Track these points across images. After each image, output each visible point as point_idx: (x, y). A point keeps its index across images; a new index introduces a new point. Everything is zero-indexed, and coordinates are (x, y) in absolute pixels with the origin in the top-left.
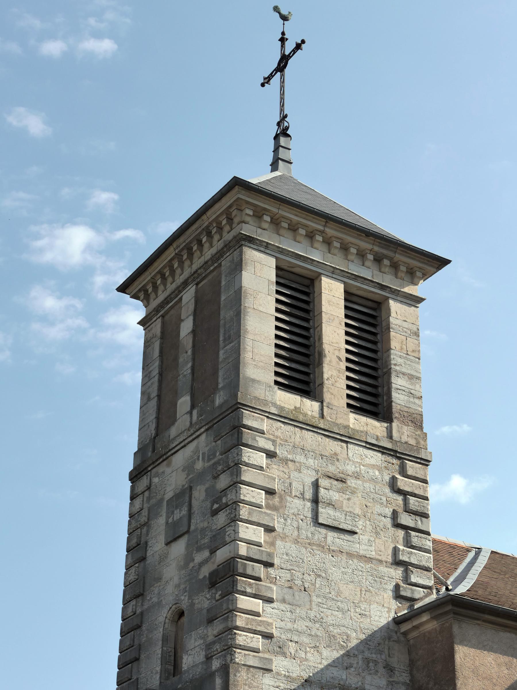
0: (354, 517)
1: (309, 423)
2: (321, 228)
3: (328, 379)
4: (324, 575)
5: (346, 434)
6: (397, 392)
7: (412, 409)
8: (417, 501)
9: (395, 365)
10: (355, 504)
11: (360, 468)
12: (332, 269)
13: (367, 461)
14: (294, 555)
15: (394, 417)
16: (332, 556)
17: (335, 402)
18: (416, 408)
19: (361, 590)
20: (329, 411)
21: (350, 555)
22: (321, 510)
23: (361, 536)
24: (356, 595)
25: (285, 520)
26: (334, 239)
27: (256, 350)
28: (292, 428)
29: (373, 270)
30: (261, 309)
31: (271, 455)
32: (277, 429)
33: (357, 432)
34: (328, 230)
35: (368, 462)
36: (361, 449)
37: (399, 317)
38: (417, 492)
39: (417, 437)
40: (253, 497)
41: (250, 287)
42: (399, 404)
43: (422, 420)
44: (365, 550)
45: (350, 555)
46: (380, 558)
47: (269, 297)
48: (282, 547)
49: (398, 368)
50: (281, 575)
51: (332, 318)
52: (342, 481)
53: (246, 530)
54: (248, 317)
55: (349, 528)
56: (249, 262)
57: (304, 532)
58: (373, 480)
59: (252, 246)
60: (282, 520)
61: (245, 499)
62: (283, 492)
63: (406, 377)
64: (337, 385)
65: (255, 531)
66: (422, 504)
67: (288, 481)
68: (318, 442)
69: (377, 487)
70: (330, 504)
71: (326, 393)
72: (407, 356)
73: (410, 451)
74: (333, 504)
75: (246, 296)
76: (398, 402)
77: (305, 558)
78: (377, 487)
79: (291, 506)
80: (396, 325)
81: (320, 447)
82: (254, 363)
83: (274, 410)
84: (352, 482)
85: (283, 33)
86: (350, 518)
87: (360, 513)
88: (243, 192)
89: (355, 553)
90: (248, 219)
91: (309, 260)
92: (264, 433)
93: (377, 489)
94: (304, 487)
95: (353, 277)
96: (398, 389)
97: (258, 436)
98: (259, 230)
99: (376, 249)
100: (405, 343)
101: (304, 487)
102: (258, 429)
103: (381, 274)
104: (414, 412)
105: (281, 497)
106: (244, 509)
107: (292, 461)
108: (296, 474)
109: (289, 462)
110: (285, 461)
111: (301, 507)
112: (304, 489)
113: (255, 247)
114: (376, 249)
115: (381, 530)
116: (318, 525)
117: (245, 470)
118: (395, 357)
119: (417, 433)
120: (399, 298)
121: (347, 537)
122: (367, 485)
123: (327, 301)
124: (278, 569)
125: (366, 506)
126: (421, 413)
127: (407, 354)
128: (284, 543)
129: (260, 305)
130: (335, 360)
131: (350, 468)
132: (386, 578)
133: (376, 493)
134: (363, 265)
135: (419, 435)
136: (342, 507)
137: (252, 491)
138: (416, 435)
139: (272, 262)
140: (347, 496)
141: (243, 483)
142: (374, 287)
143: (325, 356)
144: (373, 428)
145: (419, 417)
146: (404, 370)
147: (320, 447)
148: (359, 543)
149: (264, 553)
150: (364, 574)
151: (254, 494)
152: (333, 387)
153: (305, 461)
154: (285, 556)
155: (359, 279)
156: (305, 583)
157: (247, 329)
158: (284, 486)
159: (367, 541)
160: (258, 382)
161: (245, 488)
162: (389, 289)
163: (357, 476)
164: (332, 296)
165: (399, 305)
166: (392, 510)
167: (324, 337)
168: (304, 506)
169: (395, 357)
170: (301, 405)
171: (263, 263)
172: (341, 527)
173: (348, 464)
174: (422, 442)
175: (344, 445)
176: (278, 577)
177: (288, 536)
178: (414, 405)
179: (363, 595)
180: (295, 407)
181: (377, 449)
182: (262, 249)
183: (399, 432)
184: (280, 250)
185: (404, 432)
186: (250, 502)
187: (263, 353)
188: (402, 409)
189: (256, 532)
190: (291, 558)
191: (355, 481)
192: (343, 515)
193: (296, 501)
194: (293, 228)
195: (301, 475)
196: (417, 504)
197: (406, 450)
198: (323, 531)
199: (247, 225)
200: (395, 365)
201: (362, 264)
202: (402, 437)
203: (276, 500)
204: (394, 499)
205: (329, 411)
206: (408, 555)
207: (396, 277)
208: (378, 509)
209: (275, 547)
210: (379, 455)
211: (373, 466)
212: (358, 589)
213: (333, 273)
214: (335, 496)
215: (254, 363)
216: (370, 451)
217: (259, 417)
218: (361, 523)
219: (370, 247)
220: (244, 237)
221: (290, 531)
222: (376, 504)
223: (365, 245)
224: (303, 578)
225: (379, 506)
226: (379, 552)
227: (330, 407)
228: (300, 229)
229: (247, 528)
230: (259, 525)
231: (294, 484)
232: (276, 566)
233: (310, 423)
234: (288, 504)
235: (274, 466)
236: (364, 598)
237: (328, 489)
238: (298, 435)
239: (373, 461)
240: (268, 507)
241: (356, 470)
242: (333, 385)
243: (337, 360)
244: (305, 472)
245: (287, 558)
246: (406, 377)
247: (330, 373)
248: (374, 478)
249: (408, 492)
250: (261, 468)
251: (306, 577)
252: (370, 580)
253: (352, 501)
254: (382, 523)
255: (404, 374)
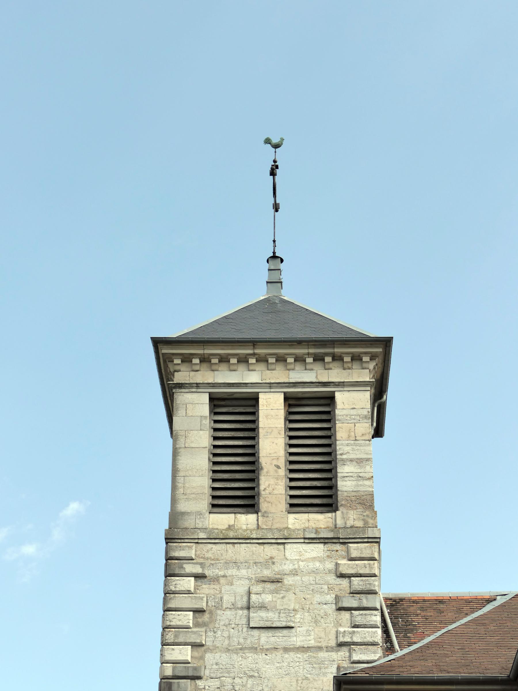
0: (289, 613)
1: (240, 537)
2: (250, 352)
3: (265, 489)
4: (256, 674)
5: (281, 537)
6: (343, 481)
7: (361, 491)
8: (362, 580)
9: (341, 454)
10: (289, 600)
11: (299, 565)
12: (268, 385)
13: (308, 555)
14: (224, 663)
15: (339, 505)
16: (266, 655)
17: (272, 509)
18: (364, 490)
19: (297, 680)
20: (264, 520)
21: (286, 650)
22: (252, 615)
23: (298, 629)
24: (291, 685)
25: (215, 632)
26: (268, 357)
27: (187, 485)
28: (223, 546)
29: (317, 371)
30: (193, 445)
31: (199, 577)
32: (208, 551)
33: (294, 531)
34: (257, 351)
35: (308, 556)
36: (298, 545)
37: (347, 406)
38: (361, 572)
39: (365, 518)
40: (180, 620)
41: (181, 429)
42: (346, 491)
43: (373, 500)
44: (303, 641)
45: (286, 650)
46: (319, 645)
47: (201, 432)
48: (212, 658)
49: (344, 457)
50: (210, 684)
51: (270, 431)
52: (278, 582)
53: (172, 652)
54: (179, 457)
55: (284, 624)
56: (181, 406)
57: (235, 639)
58: (315, 572)
59: (183, 390)
60: (212, 633)
61: (172, 624)
62: (213, 607)
63: (354, 463)
64: (275, 492)
65: (181, 651)
66: (367, 582)
67: (219, 596)
68: (252, 551)
69: (318, 578)
70: (262, 607)
71: (262, 504)
72: (356, 442)
73: (354, 534)
74: (266, 606)
75: (177, 438)
76: (345, 489)
77: (236, 663)
78: (317, 577)
79: (222, 618)
80: (343, 416)
81: (254, 556)
82: (185, 497)
83: (202, 535)
84: (288, 581)
85: (275, 161)
86: (284, 615)
87: (297, 608)
88: (165, 347)
89: (291, 647)
90: (177, 368)
91: (242, 385)
92: (192, 559)
93: (317, 580)
94: (235, 598)
95: (292, 385)
96: (344, 477)
97: (187, 563)
98: (192, 373)
99: (312, 351)
100: (353, 430)
101: (235, 598)
102: (185, 557)
103: (327, 371)
104: (363, 494)
105: (211, 613)
106: (170, 634)
107: (223, 576)
108: (228, 587)
109: (221, 579)
110: (216, 579)
111: (232, 617)
112: (235, 599)
113: (187, 390)
114: (312, 351)
115: (322, 618)
116: (251, 629)
117: (171, 599)
118: (341, 447)
119: (365, 514)
120: (346, 389)
121: (285, 632)
122: (306, 579)
123: (264, 417)
124: (207, 680)
125: (304, 599)
126: (371, 493)
127: (356, 440)
128: (214, 654)
129: (192, 442)
130: (272, 469)
131: (288, 567)
132: (326, 663)
133: (316, 584)
134: (306, 369)
135: (368, 516)
136: (275, 607)
137: (179, 615)
138: (364, 516)
139: (206, 398)
140: (282, 595)
141: (170, 609)
142: (317, 387)
143: (262, 469)
144: (316, 522)
145: (368, 497)
146: (352, 456)
147: (254, 556)
148: (296, 636)
149: (189, 669)
150: (302, 664)
151: (181, 617)
152: (270, 496)
153: (237, 573)
154: (215, 667)
155: (297, 385)
156: (236, 686)
157: (178, 468)
158: (215, 602)
159: (305, 632)
160: (188, 513)
161: (171, 614)
162: (333, 384)
163: (294, 573)
164: (272, 411)
165: (347, 394)
166: (334, 596)
167: (260, 451)
168: (236, 614)
169: (341, 447)
170: (235, 522)
171: (195, 402)
172: (274, 626)
173: (285, 564)
174: (371, 521)
175: (281, 547)
176: (207, 687)
177: (218, 647)
178: (365, 486)
179: (299, 685)
180: (229, 526)
181: (318, 541)
182: (194, 390)
183: (344, 518)
184: (211, 385)
185: (349, 517)
186: (177, 625)
187: (194, 485)
188: (349, 495)
189: (182, 651)
190: (221, 666)
191: (293, 578)
192: (277, 614)
193: (228, 612)
194: (224, 360)
195: (232, 587)
196: (361, 583)
197: (350, 534)
198: (256, 632)
199: (180, 372)
200: (341, 454)
201: (304, 368)
202: (348, 522)
203: (206, 617)
204: (337, 585)
205: (264, 520)
206: (350, 635)
207: (344, 369)
208: (318, 598)
209: (204, 660)
210: (321, 546)
211: (314, 559)
212: (294, 680)
213: (270, 388)
214: (267, 598)
215: (185, 497)
216: (311, 545)
217: (187, 546)
218: (298, 616)
219: (306, 351)
220: (174, 386)
221: (221, 641)
222: (316, 594)
223: (300, 351)
224: (234, 682)
225: (319, 596)
226: (319, 640)
227: (266, 515)
228: (231, 359)
229: (173, 649)
230: (186, 644)
231: (225, 598)
232: (205, 677)
233: (242, 537)
234: (218, 617)
235: (204, 586)
236: (300, 687)
237: (260, 594)
238: (230, 551)
239: (314, 554)
240: (197, 624)
241: (294, 567)
242: (270, 494)
243: (276, 468)
244: (237, 583)
245: (217, 667)
246: (354, 463)
247: (267, 484)
248: (314, 570)
249: (352, 574)
250: (189, 592)
251: (237, 680)
252: (308, 668)
253: (287, 598)
254: (322, 611)
255: (351, 460)
